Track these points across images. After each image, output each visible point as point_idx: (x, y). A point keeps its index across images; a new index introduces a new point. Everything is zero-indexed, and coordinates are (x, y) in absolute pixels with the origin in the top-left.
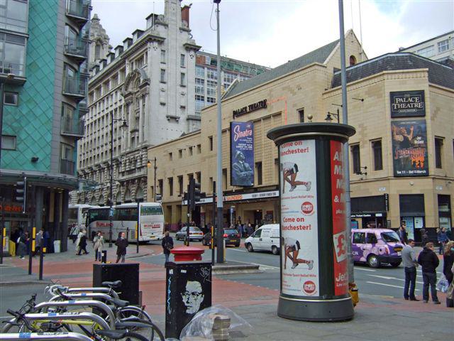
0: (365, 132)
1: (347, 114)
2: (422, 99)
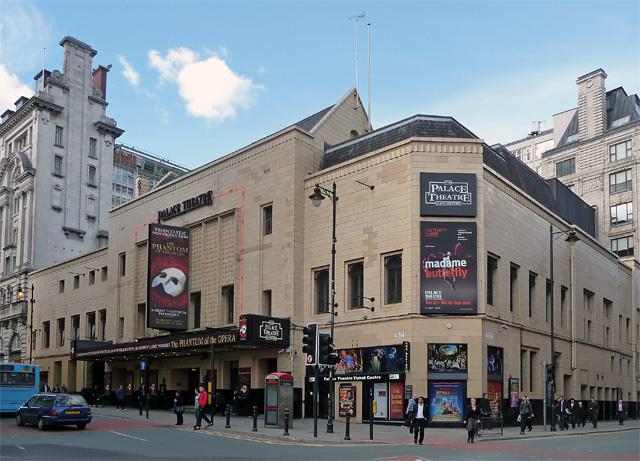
0: (375, 240)
2: (473, 189)
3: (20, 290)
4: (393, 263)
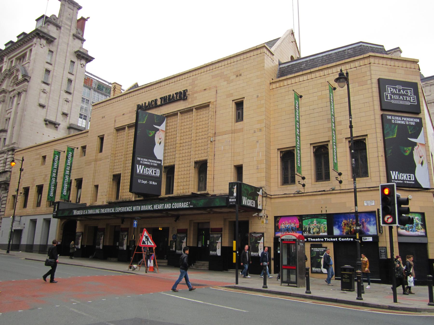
1: (397, 59)
2: (416, 93)
3: (13, 161)
4: (358, 146)
